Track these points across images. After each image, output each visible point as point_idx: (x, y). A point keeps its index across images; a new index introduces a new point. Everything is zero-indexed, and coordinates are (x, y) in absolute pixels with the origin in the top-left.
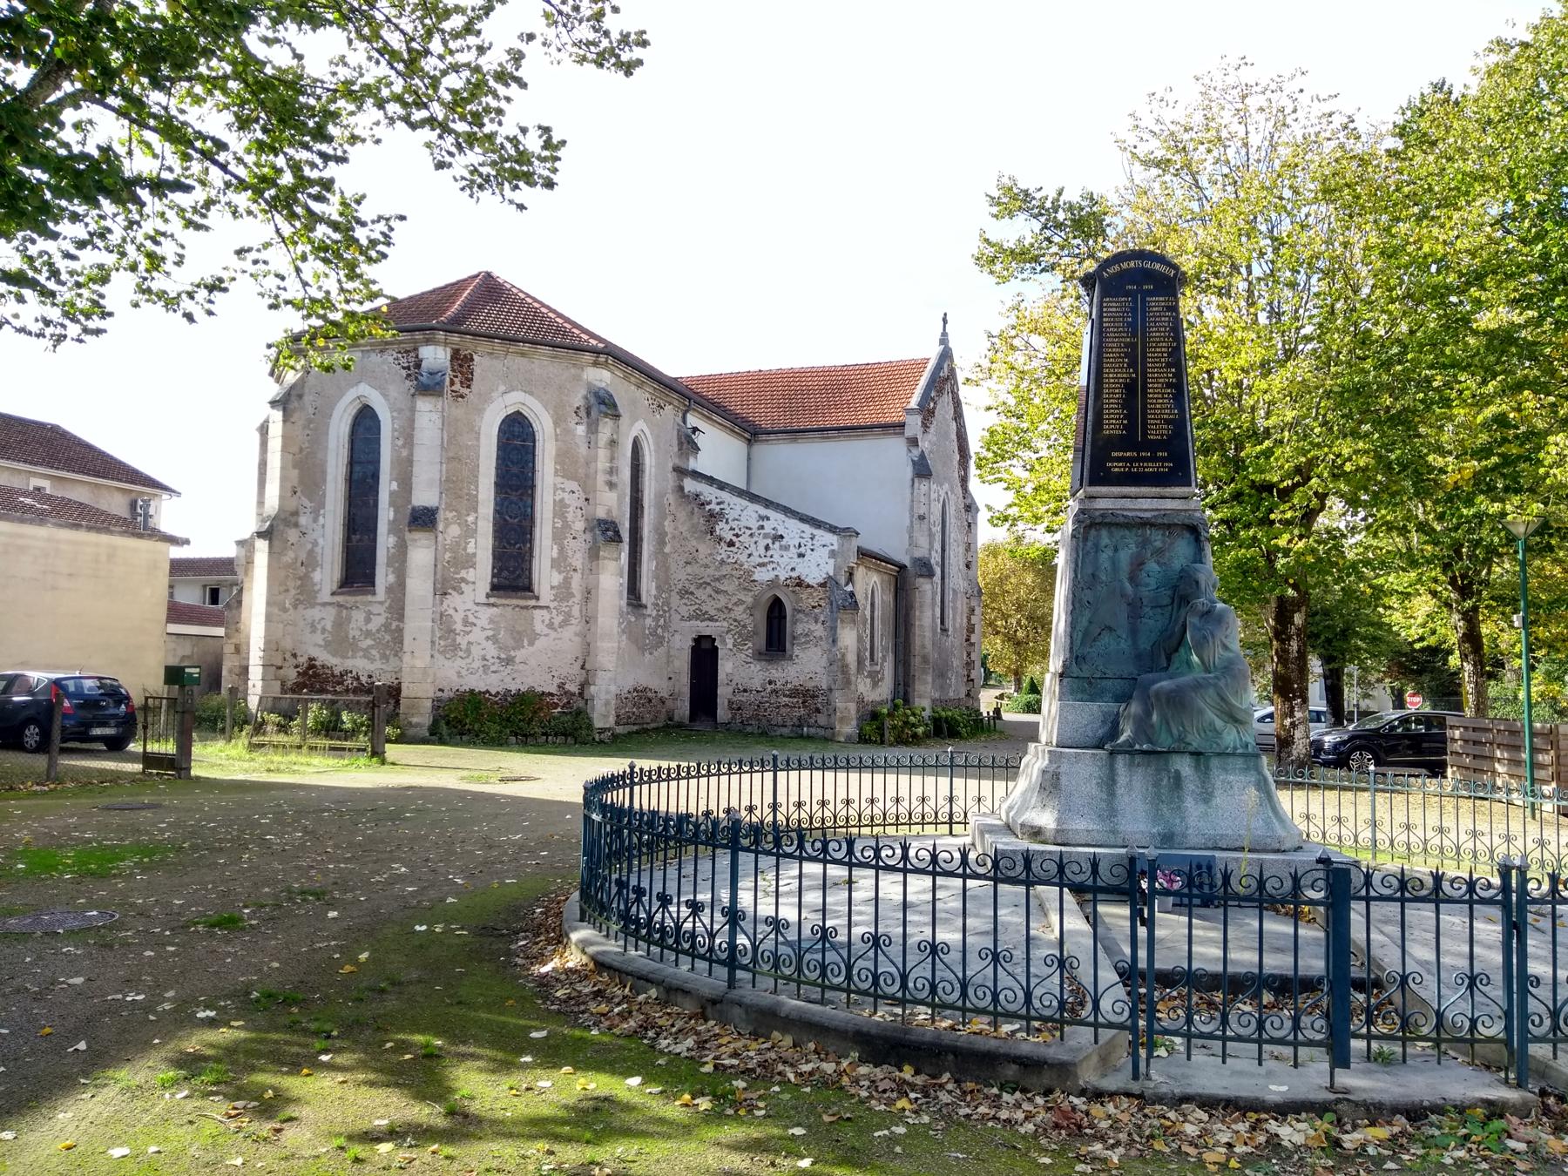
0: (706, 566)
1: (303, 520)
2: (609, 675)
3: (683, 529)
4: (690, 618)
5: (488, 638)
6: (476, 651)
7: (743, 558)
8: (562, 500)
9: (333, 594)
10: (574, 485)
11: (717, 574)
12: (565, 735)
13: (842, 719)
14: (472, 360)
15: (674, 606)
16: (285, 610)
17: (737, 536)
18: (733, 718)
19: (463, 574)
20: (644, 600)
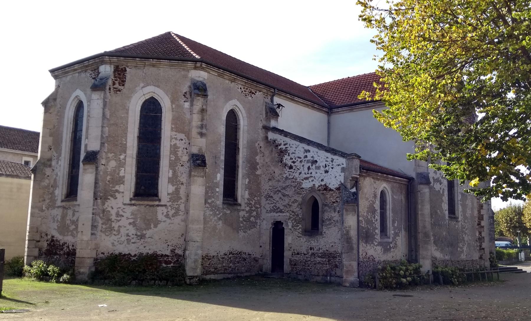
0: (279, 181)
1: (54, 163)
2: (197, 244)
3: (267, 160)
4: (271, 211)
5: (130, 224)
6: (123, 231)
7: (297, 175)
8: (175, 145)
9: (62, 201)
10: (182, 136)
11: (284, 185)
12: (167, 280)
13: (348, 272)
14: (126, 70)
15: (263, 204)
16: (42, 210)
17: (294, 162)
18: (292, 270)
19: (117, 187)
20: (239, 200)
